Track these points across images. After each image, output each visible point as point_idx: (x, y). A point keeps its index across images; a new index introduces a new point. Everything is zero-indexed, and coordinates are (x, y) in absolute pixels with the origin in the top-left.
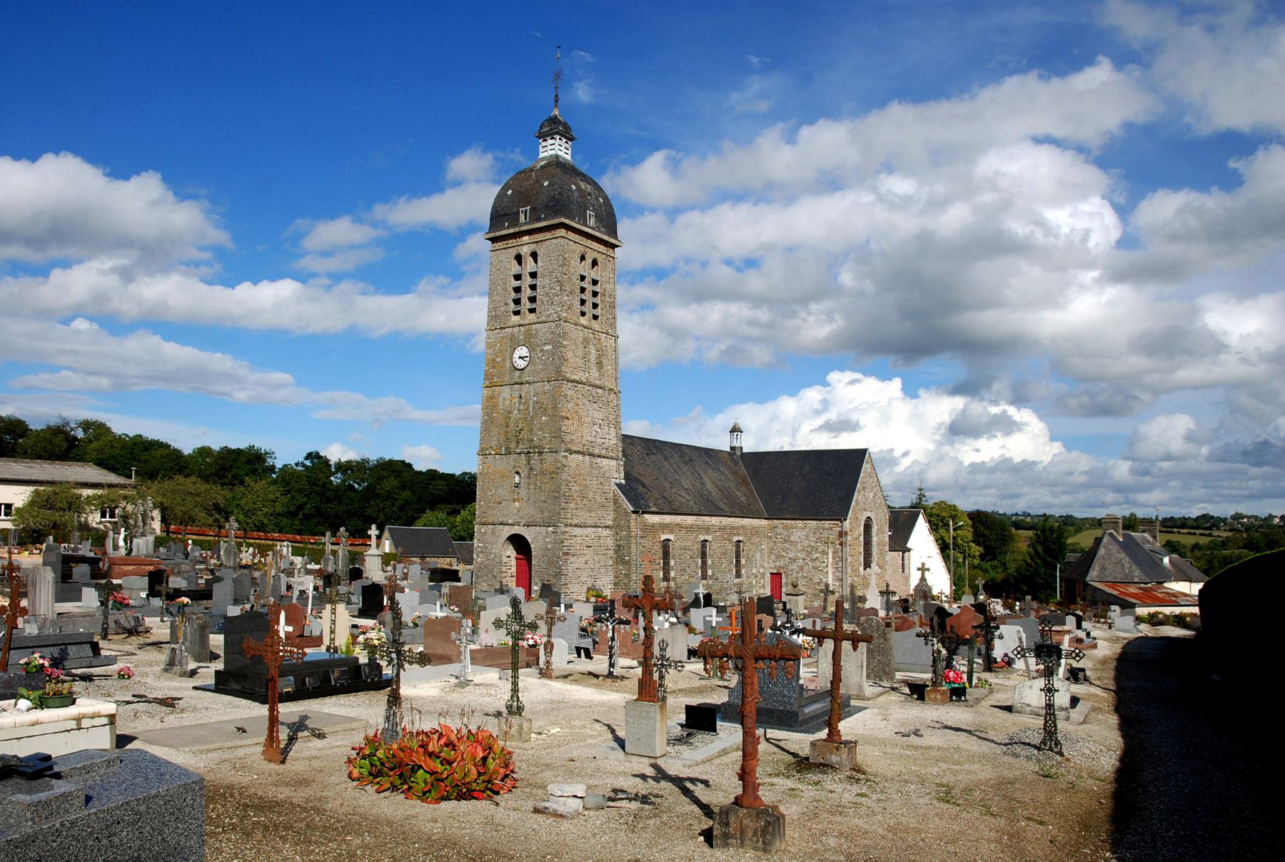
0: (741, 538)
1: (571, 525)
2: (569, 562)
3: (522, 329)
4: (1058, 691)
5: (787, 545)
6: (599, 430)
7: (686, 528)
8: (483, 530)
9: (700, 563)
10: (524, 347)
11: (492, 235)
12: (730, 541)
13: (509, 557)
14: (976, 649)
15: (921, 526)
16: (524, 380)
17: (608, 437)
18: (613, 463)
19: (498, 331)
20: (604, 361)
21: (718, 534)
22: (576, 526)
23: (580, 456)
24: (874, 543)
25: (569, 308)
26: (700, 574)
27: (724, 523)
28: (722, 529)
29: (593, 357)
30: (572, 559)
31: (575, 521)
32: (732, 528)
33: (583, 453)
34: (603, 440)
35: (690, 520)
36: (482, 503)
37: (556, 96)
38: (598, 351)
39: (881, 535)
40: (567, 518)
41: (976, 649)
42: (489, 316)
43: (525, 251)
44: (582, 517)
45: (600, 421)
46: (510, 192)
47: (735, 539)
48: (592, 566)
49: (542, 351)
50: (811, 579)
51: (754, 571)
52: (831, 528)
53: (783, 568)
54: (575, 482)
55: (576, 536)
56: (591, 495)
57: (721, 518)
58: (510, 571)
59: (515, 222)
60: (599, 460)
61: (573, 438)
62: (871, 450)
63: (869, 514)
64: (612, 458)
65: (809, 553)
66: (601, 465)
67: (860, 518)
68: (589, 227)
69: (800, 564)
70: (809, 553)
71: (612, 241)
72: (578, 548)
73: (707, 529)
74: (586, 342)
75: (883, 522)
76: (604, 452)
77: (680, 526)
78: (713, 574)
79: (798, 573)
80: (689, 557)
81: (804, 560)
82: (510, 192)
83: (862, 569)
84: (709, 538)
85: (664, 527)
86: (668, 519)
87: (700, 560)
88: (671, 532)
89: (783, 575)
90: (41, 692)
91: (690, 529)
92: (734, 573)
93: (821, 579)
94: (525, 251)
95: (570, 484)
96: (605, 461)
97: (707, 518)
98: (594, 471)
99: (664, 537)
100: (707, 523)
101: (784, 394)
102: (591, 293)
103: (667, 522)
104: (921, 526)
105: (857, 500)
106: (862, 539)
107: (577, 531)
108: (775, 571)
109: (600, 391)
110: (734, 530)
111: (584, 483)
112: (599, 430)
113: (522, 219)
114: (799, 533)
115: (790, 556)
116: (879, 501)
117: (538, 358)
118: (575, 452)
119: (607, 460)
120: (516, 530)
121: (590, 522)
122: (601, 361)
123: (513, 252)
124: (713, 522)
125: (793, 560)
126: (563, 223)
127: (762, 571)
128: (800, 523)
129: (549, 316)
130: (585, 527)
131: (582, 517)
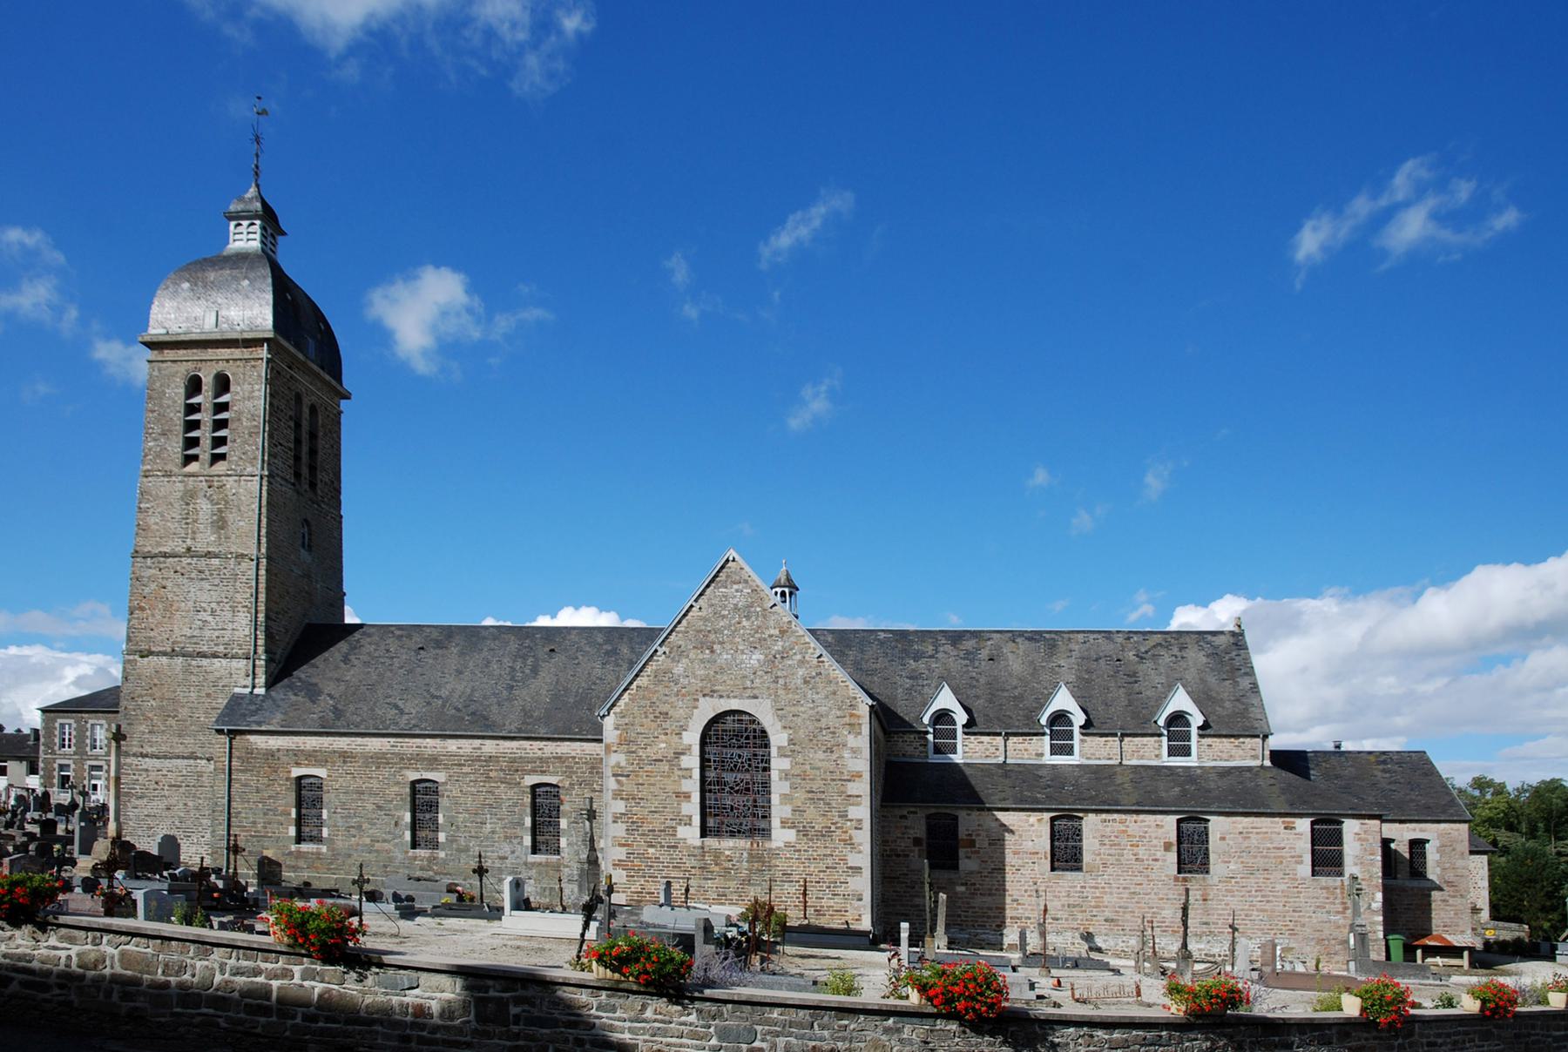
4: (1428, 841)
6: (210, 619)
11: (1084, 731)
20: (230, 517)
41: (233, 978)
44: (161, 743)
45: (214, 605)
55: (147, 770)
66: (208, 669)
73: (433, 761)
76: (221, 649)
77: (345, 756)
90: (505, 1029)
91: (379, 759)
101: (1179, 606)
107: (148, 763)
109: (215, 562)
121: (179, 750)
126: (1300, 731)
131: (161, 743)
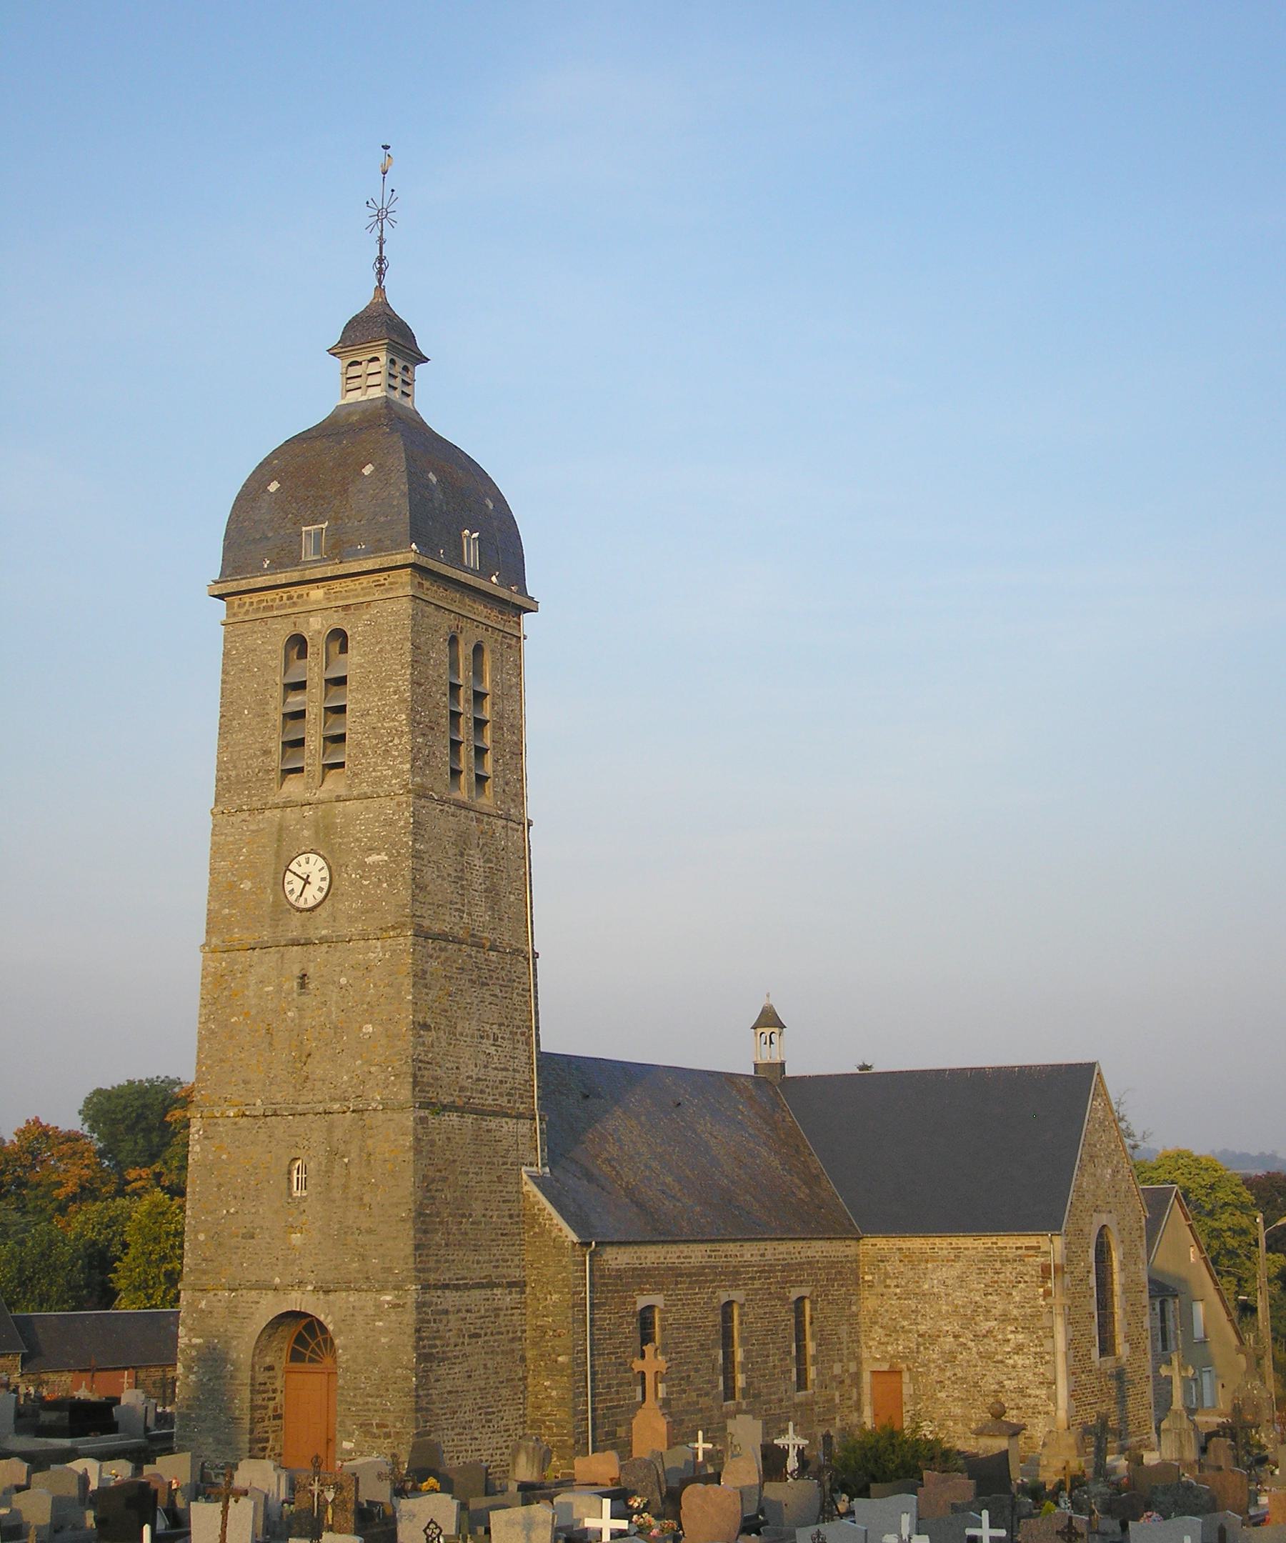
0: (805, 1291)
1: (436, 1287)
2: (432, 1377)
3: (308, 812)
5: (912, 1303)
6: (492, 1050)
7: (689, 1275)
8: (203, 1304)
9: (721, 1361)
10: (313, 857)
12: (784, 1299)
13: (270, 1368)
14: (428, 1406)
15: (1175, 1216)
16: (314, 935)
17: (512, 1065)
18: (523, 1127)
19: (245, 815)
21: (757, 1284)
22: (446, 1286)
23: (454, 1117)
24: (1117, 1288)
25: (426, 763)
26: (721, 1387)
27: (769, 1253)
28: (766, 1271)
29: (477, 879)
30: (442, 1371)
31: (446, 1277)
32: (788, 1267)
33: (460, 1110)
34: (501, 1075)
35: (696, 1254)
36: (202, 1237)
37: (381, 260)
38: (489, 861)
39: (1132, 1268)
40: (429, 1270)
41: (428, 1406)
42: (219, 780)
43: (315, 627)
46: (273, 487)
47: (794, 1294)
48: (482, 1384)
49: (363, 865)
50: (976, 1385)
51: (837, 1369)
52: (1021, 1259)
53: (904, 1358)
54: (445, 1179)
55: (446, 1312)
56: (477, 1207)
57: (762, 1245)
58: (271, 1404)
59: (295, 561)
60: (493, 1123)
61: (439, 1072)
62: (1114, 1080)
63: (1104, 1219)
64: (519, 1116)
65: (968, 1321)
67: (1086, 1230)
68: (466, 569)
69: (947, 1347)
70: (968, 1321)
71: (518, 600)
72: (452, 1341)
73: (733, 1275)
74: (462, 842)
75: (1136, 1234)
76: (503, 1101)
78: (749, 1384)
79: (942, 1370)
80: (696, 1346)
81: (956, 1337)
82: (273, 487)
83: (1095, 1352)
84: (738, 1295)
85: (642, 1277)
86: (652, 1256)
87: (721, 1351)
88: (658, 1288)
89: (906, 1377)
91: (697, 1276)
92: (794, 1378)
93: (1000, 1383)
94: (315, 627)
95: (433, 1187)
96: (508, 1125)
97: (732, 1248)
98: (484, 1150)
99: (642, 1302)
100: (734, 1261)
102: (471, 724)
103: (648, 1263)
104: (1175, 1216)
105: (1080, 1187)
106: (1093, 1278)
108: (885, 1367)
110: (792, 1271)
111: (462, 1180)
112: (492, 1050)
113: (308, 554)
114: (944, 1273)
115: (922, 1328)
116: (1124, 1186)
117: (352, 883)
118: (445, 1108)
119: (511, 1122)
120: (297, 1301)
122: (494, 885)
123: (284, 630)
124: (747, 1257)
125: (930, 1339)
127: (853, 1367)
128: (942, 1244)
129: (378, 782)
130: (467, 1287)
